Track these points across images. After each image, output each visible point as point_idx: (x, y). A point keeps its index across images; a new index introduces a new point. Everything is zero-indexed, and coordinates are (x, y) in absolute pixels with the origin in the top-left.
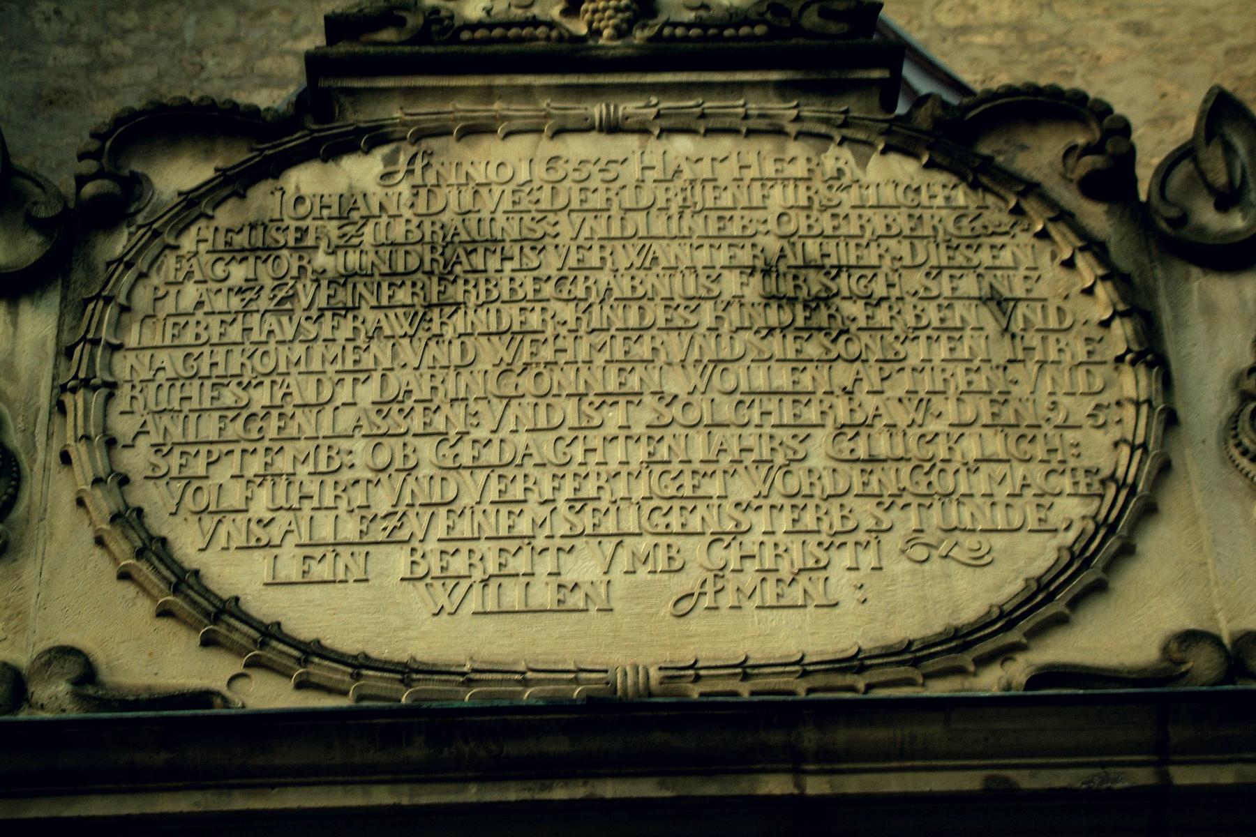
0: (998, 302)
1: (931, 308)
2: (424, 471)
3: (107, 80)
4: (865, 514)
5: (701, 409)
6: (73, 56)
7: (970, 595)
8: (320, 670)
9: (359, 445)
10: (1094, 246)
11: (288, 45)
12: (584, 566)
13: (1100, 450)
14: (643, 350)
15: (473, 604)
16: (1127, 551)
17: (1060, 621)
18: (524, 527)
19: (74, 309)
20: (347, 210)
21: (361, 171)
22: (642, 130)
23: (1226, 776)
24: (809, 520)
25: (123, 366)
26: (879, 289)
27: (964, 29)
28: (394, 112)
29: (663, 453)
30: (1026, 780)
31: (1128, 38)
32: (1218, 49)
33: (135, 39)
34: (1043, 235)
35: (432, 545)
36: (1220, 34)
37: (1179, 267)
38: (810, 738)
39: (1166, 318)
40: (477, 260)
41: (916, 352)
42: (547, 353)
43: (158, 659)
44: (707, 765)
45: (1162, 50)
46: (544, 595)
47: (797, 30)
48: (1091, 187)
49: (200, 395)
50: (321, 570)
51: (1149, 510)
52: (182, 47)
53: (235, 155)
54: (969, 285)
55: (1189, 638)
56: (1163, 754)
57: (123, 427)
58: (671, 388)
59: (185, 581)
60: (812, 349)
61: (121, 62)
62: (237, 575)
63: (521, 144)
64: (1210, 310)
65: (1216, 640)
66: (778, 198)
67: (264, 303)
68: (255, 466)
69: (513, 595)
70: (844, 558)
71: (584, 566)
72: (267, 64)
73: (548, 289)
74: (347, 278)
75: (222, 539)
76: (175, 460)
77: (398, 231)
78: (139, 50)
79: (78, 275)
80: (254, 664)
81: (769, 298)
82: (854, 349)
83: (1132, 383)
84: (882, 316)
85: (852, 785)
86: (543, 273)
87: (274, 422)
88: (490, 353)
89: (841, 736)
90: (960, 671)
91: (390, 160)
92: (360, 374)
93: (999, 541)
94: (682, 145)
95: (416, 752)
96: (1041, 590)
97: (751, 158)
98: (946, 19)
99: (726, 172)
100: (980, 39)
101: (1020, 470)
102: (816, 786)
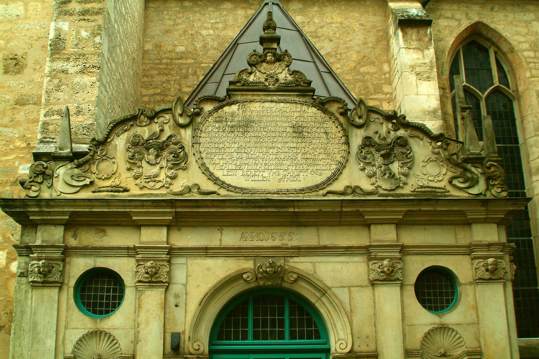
0: (326, 133)
1: (317, 134)
2: (244, 158)
3: (176, 27)
4: (305, 167)
5: (283, 150)
6: (171, 22)
7: (319, 180)
8: (230, 188)
9: (235, 154)
10: (341, 125)
11: (209, 21)
12: (266, 174)
13: (338, 158)
14: (275, 140)
15: (251, 179)
16: (341, 173)
17: (331, 184)
18: (258, 168)
20: (233, 115)
21: (234, 108)
22: (276, 102)
23: (349, 210)
24: (298, 168)
25: (201, 140)
26: (309, 131)
27: (331, 23)
28: (239, 98)
29: (278, 157)
30: (324, 210)
31: (360, 26)
32: (375, 30)
33: (182, 19)
34: (333, 122)
35: (245, 170)
36: (376, 27)
37: (352, 127)
38: (296, 204)
39: (350, 136)
40: (252, 124)
41: (314, 141)
42: (261, 140)
43: (208, 186)
44: (282, 207)
45: (366, 29)
47: (299, 85)
48: (342, 114)
49: (213, 145)
50: (230, 173)
52: (190, 21)
53: (216, 105)
54: (322, 130)
55: (348, 187)
58: (279, 146)
59: (211, 174)
60: (299, 141)
61: (179, 24)
62: (218, 174)
63: (258, 104)
64: (356, 135)
65: (351, 187)
66: (296, 114)
67: (221, 130)
68: (220, 157)
69: (256, 178)
70: (302, 174)
71: (266, 174)
72: (205, 25)
73: (262, 129)
74: (232, 127)
75: (216, 168)
76: (209, 155)
77: (240, 119)
78: (182, 21)
79: (194, 124)
80: (221, 187)
81: (294, 132)
82: (305, 141)
84: (310, 135)
85: (301, 210)
86: (261, 126)
87: (223, 150)
88: (254, 139)
90: (317, 191)
91: (239, 106)
92: (235, 143)
93: (324, 172)
94: (282, 104)
95: (244, 204)
96: (329, 179)
97: (292, 107)
98: (328, 21)
99: (288, 110)
100: (334, 25)
101: (327, 160)
102: (296, 210)
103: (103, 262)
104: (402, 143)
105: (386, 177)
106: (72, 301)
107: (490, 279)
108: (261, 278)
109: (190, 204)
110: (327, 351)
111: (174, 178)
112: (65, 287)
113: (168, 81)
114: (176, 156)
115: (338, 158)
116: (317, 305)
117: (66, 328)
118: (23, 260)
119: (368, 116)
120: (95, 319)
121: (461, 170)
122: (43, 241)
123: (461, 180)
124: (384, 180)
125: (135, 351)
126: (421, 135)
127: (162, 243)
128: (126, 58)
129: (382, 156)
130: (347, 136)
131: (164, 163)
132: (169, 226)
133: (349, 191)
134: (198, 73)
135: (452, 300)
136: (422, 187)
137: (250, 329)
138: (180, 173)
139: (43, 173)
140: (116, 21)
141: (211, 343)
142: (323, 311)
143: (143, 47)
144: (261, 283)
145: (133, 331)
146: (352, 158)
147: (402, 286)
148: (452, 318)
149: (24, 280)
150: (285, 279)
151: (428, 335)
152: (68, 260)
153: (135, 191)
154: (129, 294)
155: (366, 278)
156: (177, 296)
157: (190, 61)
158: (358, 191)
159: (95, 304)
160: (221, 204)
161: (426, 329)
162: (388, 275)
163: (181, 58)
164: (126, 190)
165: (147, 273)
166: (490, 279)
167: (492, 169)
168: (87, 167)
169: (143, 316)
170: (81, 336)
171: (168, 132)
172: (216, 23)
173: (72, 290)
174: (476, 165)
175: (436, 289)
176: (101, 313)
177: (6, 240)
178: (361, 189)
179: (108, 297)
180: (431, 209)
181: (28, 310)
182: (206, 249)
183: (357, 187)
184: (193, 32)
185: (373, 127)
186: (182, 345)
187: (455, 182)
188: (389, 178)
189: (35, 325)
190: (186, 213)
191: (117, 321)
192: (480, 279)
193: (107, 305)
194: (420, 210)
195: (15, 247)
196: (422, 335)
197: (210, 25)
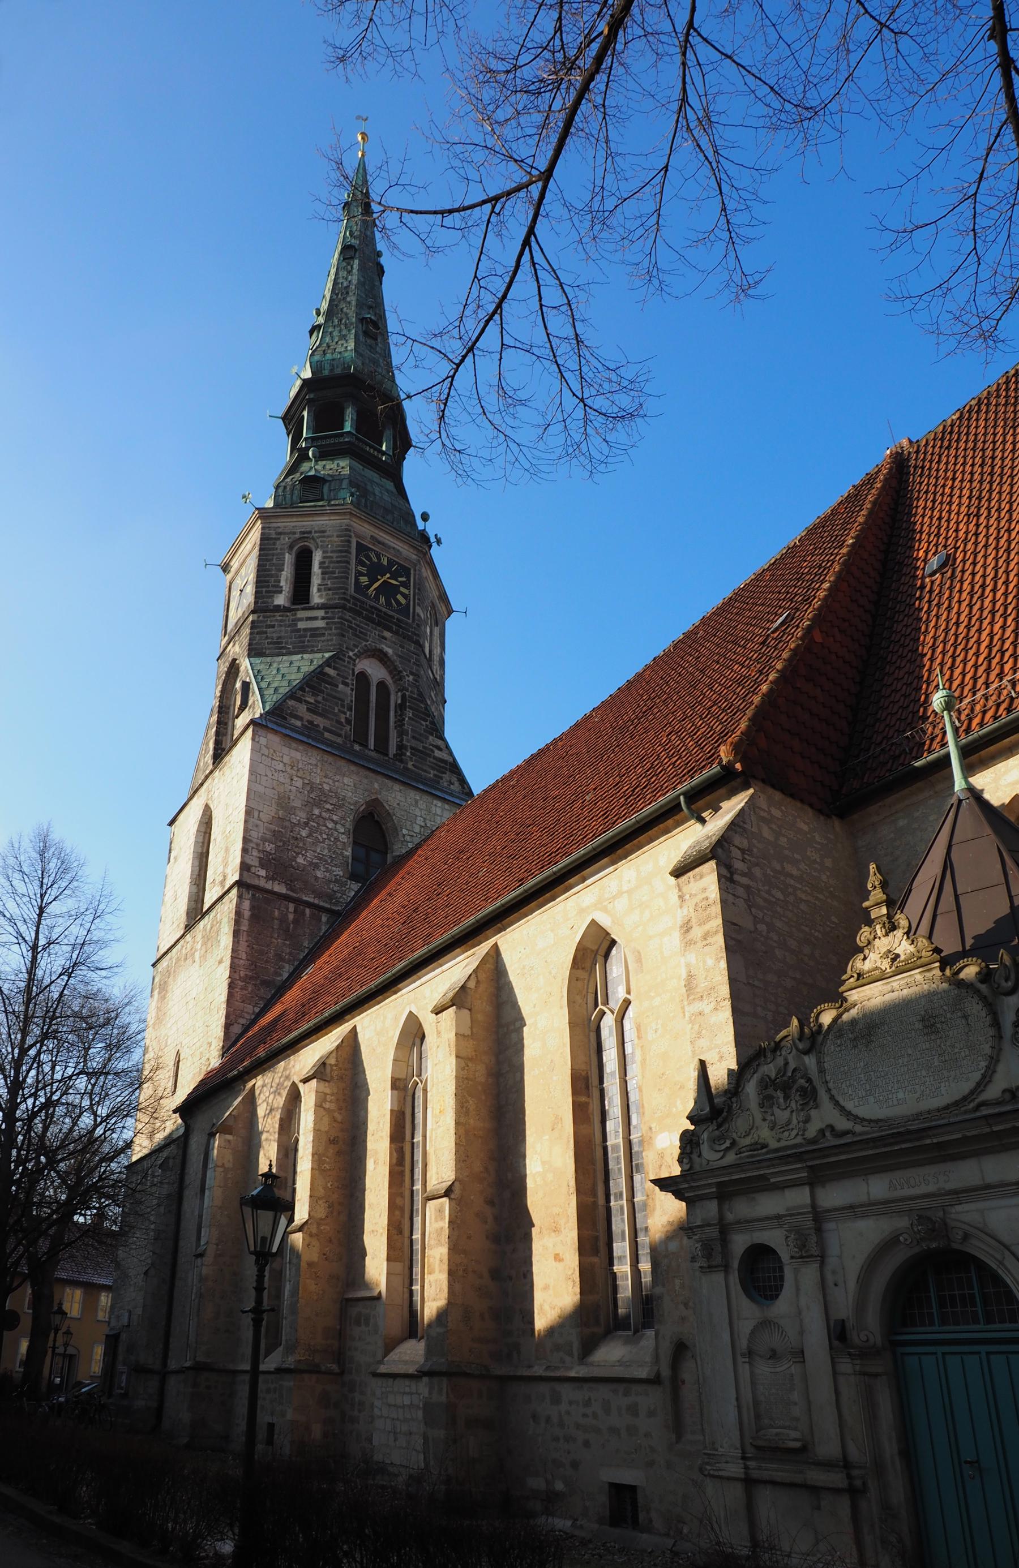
0: (965, 1017)
7: (966, 1087)
30: (968, 1134)
43: (842, 1124)
46: (895, 1103)
51: (998, 1061)
55: (1004, 1091)
56: (990, 1126)
57: (828, 1078)
62: (849, 1106)
70: (943, 1085)
71: (901, 1095)
81: (926, 1027)
83: (991, 1032)
85: (940, 1139)
96: (978, 1084)
102: (935, 1141)
114: (803, 1092)
115: (987, 1050)
116: (1000, 1272)
131: (793, 1105)
133: (1007, 1096)
138: (813, 1113)
146: (1007, 1045)
153: (773, 1144)
154: (788, 1273)
170: (751, 1328)
182: (851, 1207)
191: (782, 1306)
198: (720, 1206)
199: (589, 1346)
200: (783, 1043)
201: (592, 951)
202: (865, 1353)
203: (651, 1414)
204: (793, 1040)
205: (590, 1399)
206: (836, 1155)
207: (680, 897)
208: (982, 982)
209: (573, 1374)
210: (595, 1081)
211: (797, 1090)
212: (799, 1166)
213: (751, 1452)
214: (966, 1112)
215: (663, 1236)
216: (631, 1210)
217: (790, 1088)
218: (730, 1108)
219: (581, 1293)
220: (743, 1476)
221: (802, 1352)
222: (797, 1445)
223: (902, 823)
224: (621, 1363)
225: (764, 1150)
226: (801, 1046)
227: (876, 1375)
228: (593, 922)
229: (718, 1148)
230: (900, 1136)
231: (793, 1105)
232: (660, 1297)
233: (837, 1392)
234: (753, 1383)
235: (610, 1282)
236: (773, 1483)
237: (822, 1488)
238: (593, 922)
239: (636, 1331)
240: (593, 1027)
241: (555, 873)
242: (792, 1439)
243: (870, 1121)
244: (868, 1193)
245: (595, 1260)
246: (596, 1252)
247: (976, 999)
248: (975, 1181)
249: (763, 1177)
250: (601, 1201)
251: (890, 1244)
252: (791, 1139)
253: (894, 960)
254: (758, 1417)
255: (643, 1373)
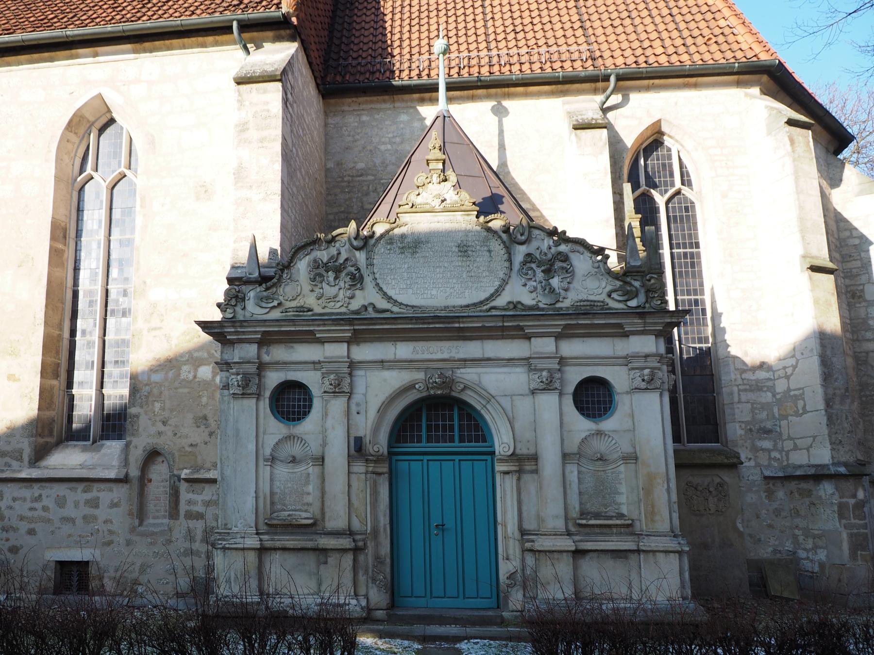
0: (490, 251)
4: (470, 284)
6: (350, 139)
7: (483, 296)
10: (504, 242)
12: (434, 292)
19: (368, 252)
30: (487, 325)
41: (478, 259)
43: (382, 304)
44: (449, 323)
46: (429, 296)
55: (509, 303)
57: (375, 271)
59: (385, 294)
62: (391, 293)
71: (434, 292)
72: (383, 140)
81: (460, 251)
83: (507, 264)
85: (466, 325)
88: (422, 260)
89: (465, 320)
92: (405, 263)
95: (414, 321)
96: (492, 295)
102: (462, 325)
103: (293, 376)
104: (565, 258)
105: (546, 292)
106: (268, 410)
107: (544, 389)
108: (432, 388)
109: (366, 322)
110: (493, 453)
111: (352, 297)
112: (262, 398)
113: (350, 199)
114: (353, 277)
115: (501, 275)
116: (483, 412)
117: (264, 434)
118: (225, 374)
119: (530, 232)
120: (289, 426)
121: (621, 283)
122: (240, 358)
123: (620, 293)
124: (544, 295)
125: (323, 453)
126: (581, 249)
127: (343, 357)
128: (307, 180)
129: (542, 271)
130: (509, 254)
131: (342, 284)
132: (349, 342)
133: (511, 306)
134: (378, 190)
135: (610, 408)
136: (581, 301)
137: (424, 433)
138: (358, 293)
139: (237, 297)
140: (293, 145)
141: (390, 446)
142: (488, 417)
143: (325, 165)
144: (432, 392)
145: (321, 436)
146: (514, 274)
147: (561, 395)
148: (608, 424)
149: (226, 392)
150: (453, 388)
151: (584, 440)
152: (263, 373)
153: (318, 310)
154: (317, 404)
155: (527, 387)
156: (358, 405)
157: (370, 178)
158: (519, 306)
159: (288, 412)
160: (393, 321)
161: (583, 435)
162: (547, 384)
163: (361, 175)
164: (310, 310)
165: (331, 384)
166: (544, 389)
167: (653, 281)
168: (275, 289)
169: (329, 423)
170: (277, 440)
171: (344, 256)
172: (394, 137)
173: (267, 401)
174: (636, 278)
175: (593, 397)
176: (294, 420)
177: (211, 355)
178: (522, 304)
179: (299, 406)
180: (589, 322)
181: (231, 418)
182: (382, 362)
183: (519, 302)
184: (371, 148)
185: (535, 244)
186: (364, 448)
187: (614, 295)
188: (549, 292)
189: (237, 431)
190: (364, 327)
191: (308, 426)
192: (636, 389)
193: (299, 413)
194: (578, 324)
195: (216, 363)
196: (580, 440)
197: (387, 140)
198: (259, 349)
199: (40, 453)
200: (337, 238)
201: (88, 121)
202: (379, 459)
203: (114, 505)
204: (349, 239)
205: (40, 496)
206: (382, 324)
207: (238, 101)
208: (504, 232)
209: (23, 475)
210: (72, 233)
211: (347, 274)
212: (348, 328)
213: (263, 528)
214: (481, 311)
215: (146, 369)
216: (101, 345)
217: (340, 271)
218: (281, 276)
219: (39, 409)
220: (259, 546)
221: (323, 459)
222: (310, 522)
223: (364, 118)
224: (82, 466)
225: (310, 313)
226: (355, 243)
227: (380, 474)
228: (100, 96)
229: (264, 305)
230: (437, 318)
231: (342, 284)
232: (137, 416)
233: (349, 486)
234: (272, 480)
235: (66, 401)
236: (284, 549)
237: (331, 549)
238: (100, 96)
239: (94, 442)
240: (77, 186)
241: (67, 37)
242: (304, 517)
243: (407, 306)
244: (395, 354)
245: (55, 382)
246: (56, 376)
247: (499, 241)
248: (478, 354)
249: (312, 332)
250: (66, 334)
251: (411, 387)
252: (335, 308)
253: (443, 201)
254: (272, 503)
255: (112, 475)
